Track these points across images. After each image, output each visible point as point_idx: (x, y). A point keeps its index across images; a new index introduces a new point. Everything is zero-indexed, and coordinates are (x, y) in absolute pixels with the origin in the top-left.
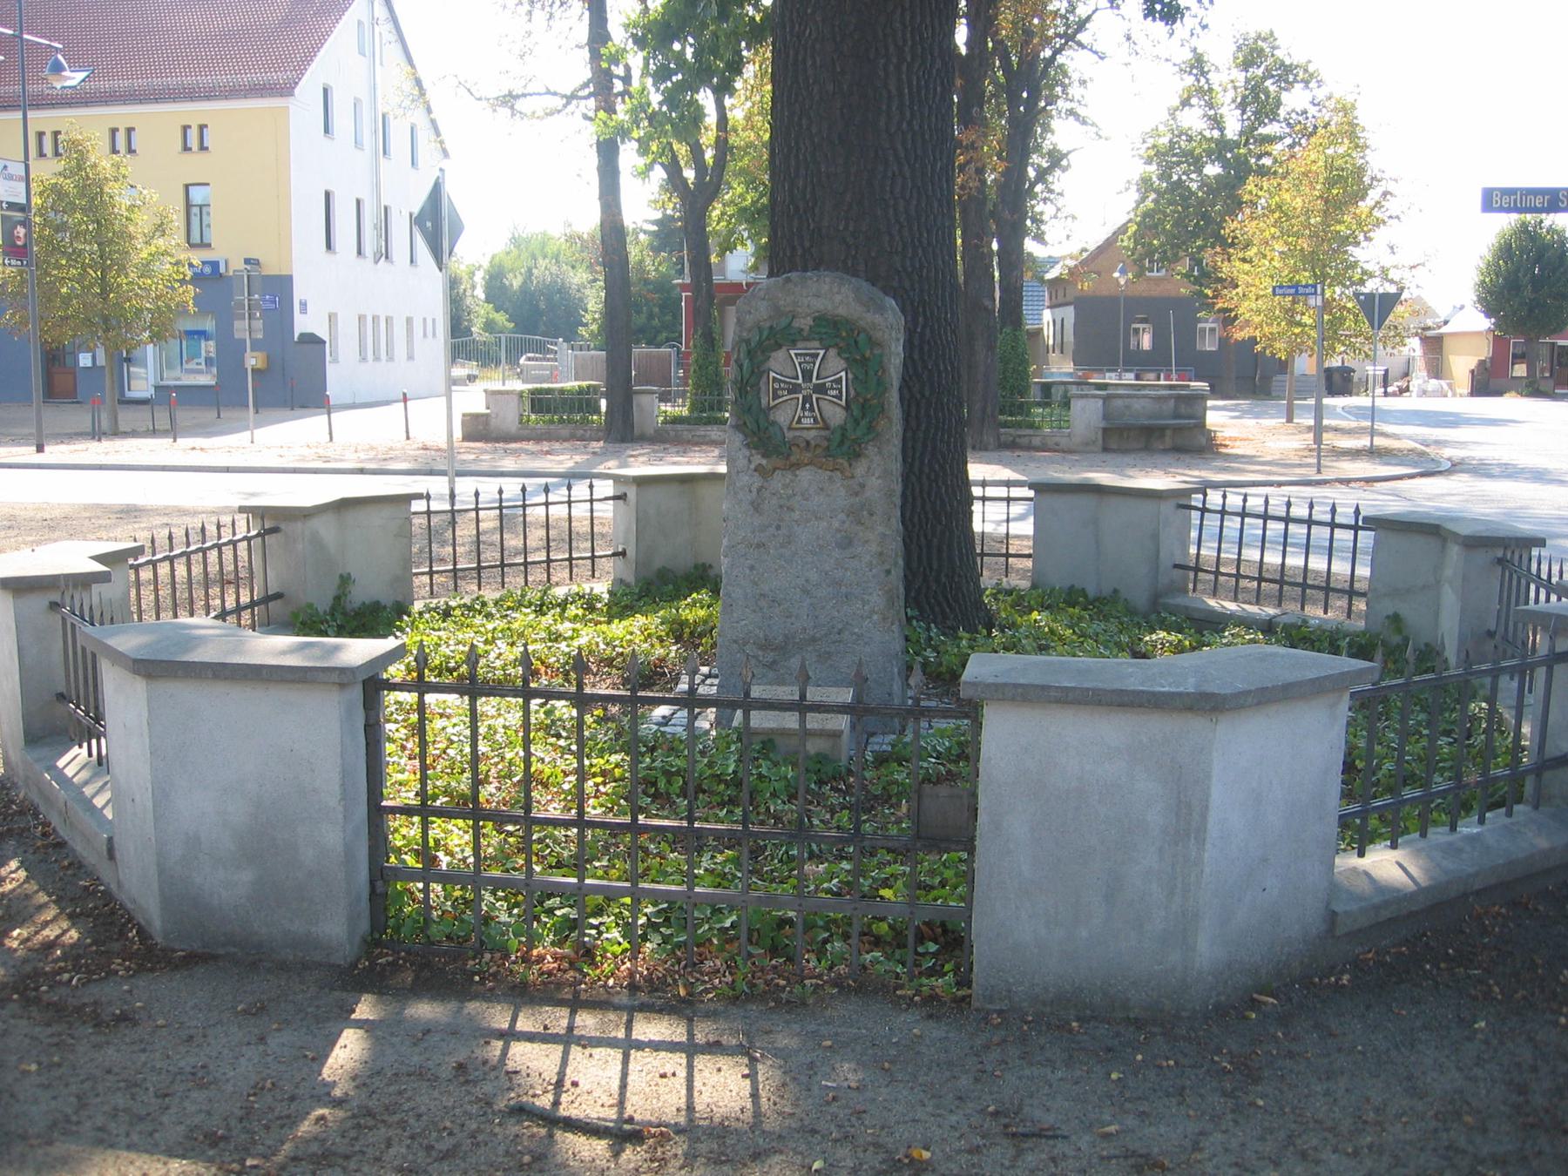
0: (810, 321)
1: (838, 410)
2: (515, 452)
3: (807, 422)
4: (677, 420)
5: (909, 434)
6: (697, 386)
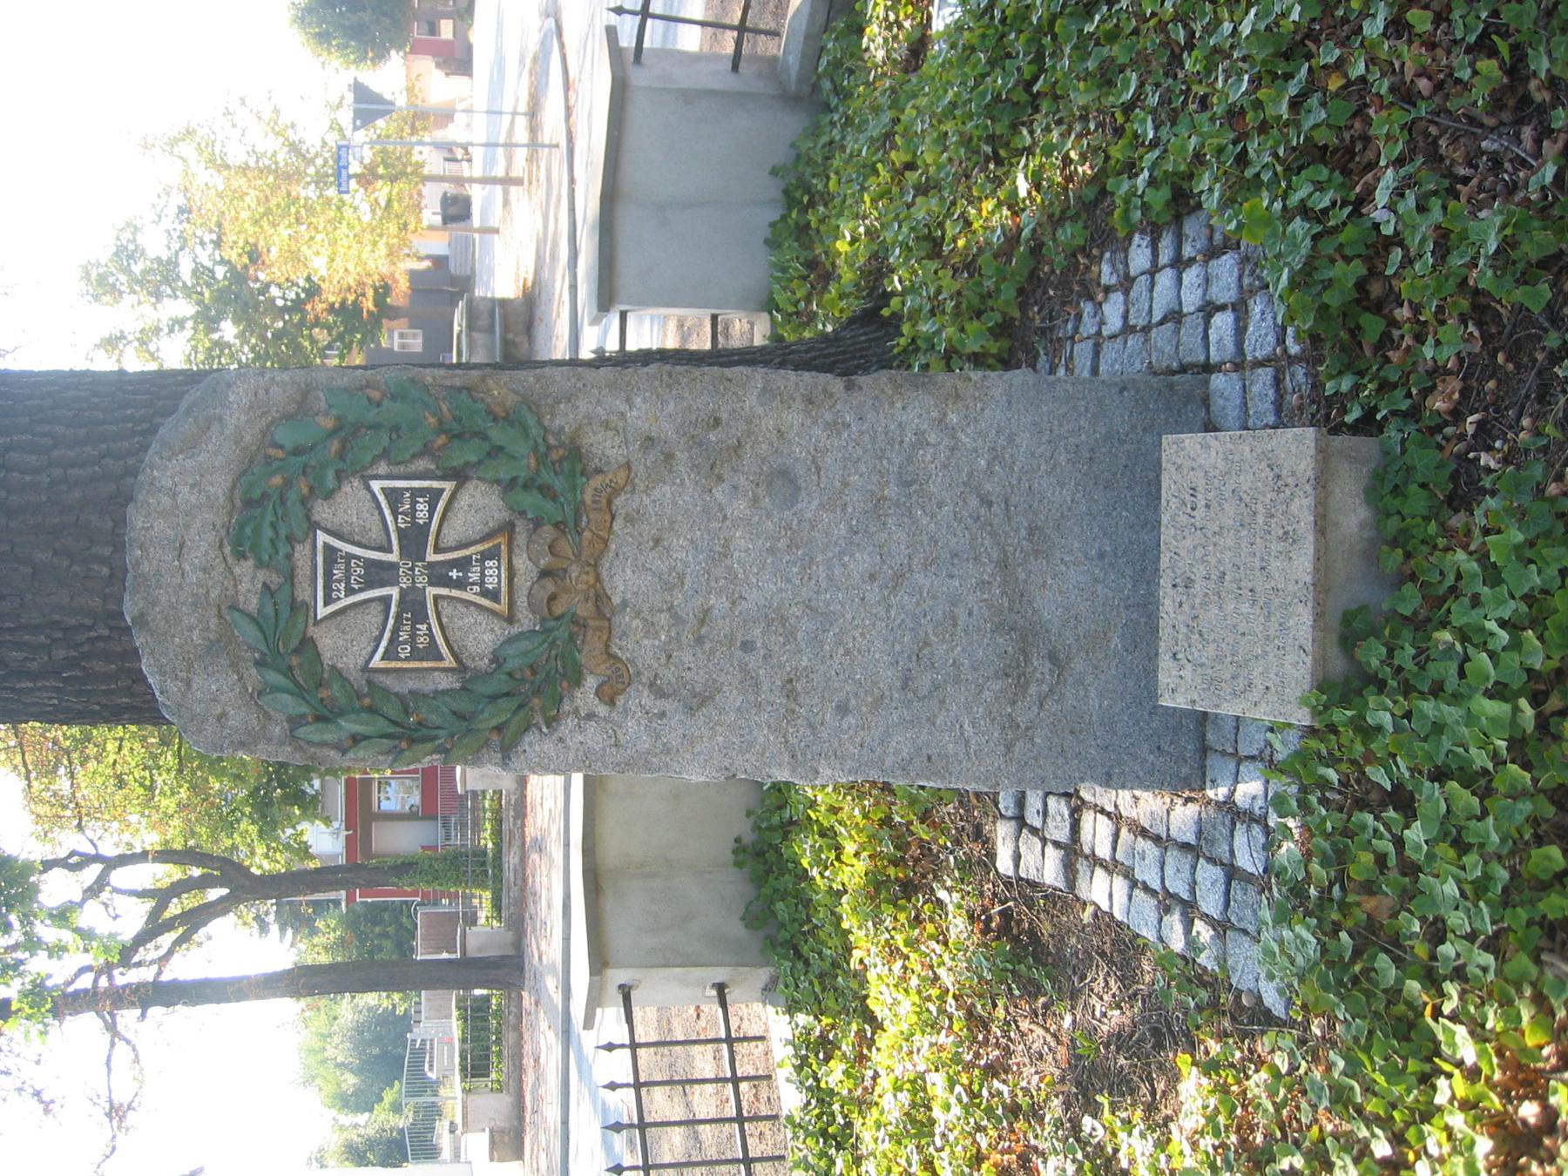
0: (245, 569)
1: (464, 500)
2: (537, 1099)
3: (494, 574)
4: (497, 905)
6: (457, 882)
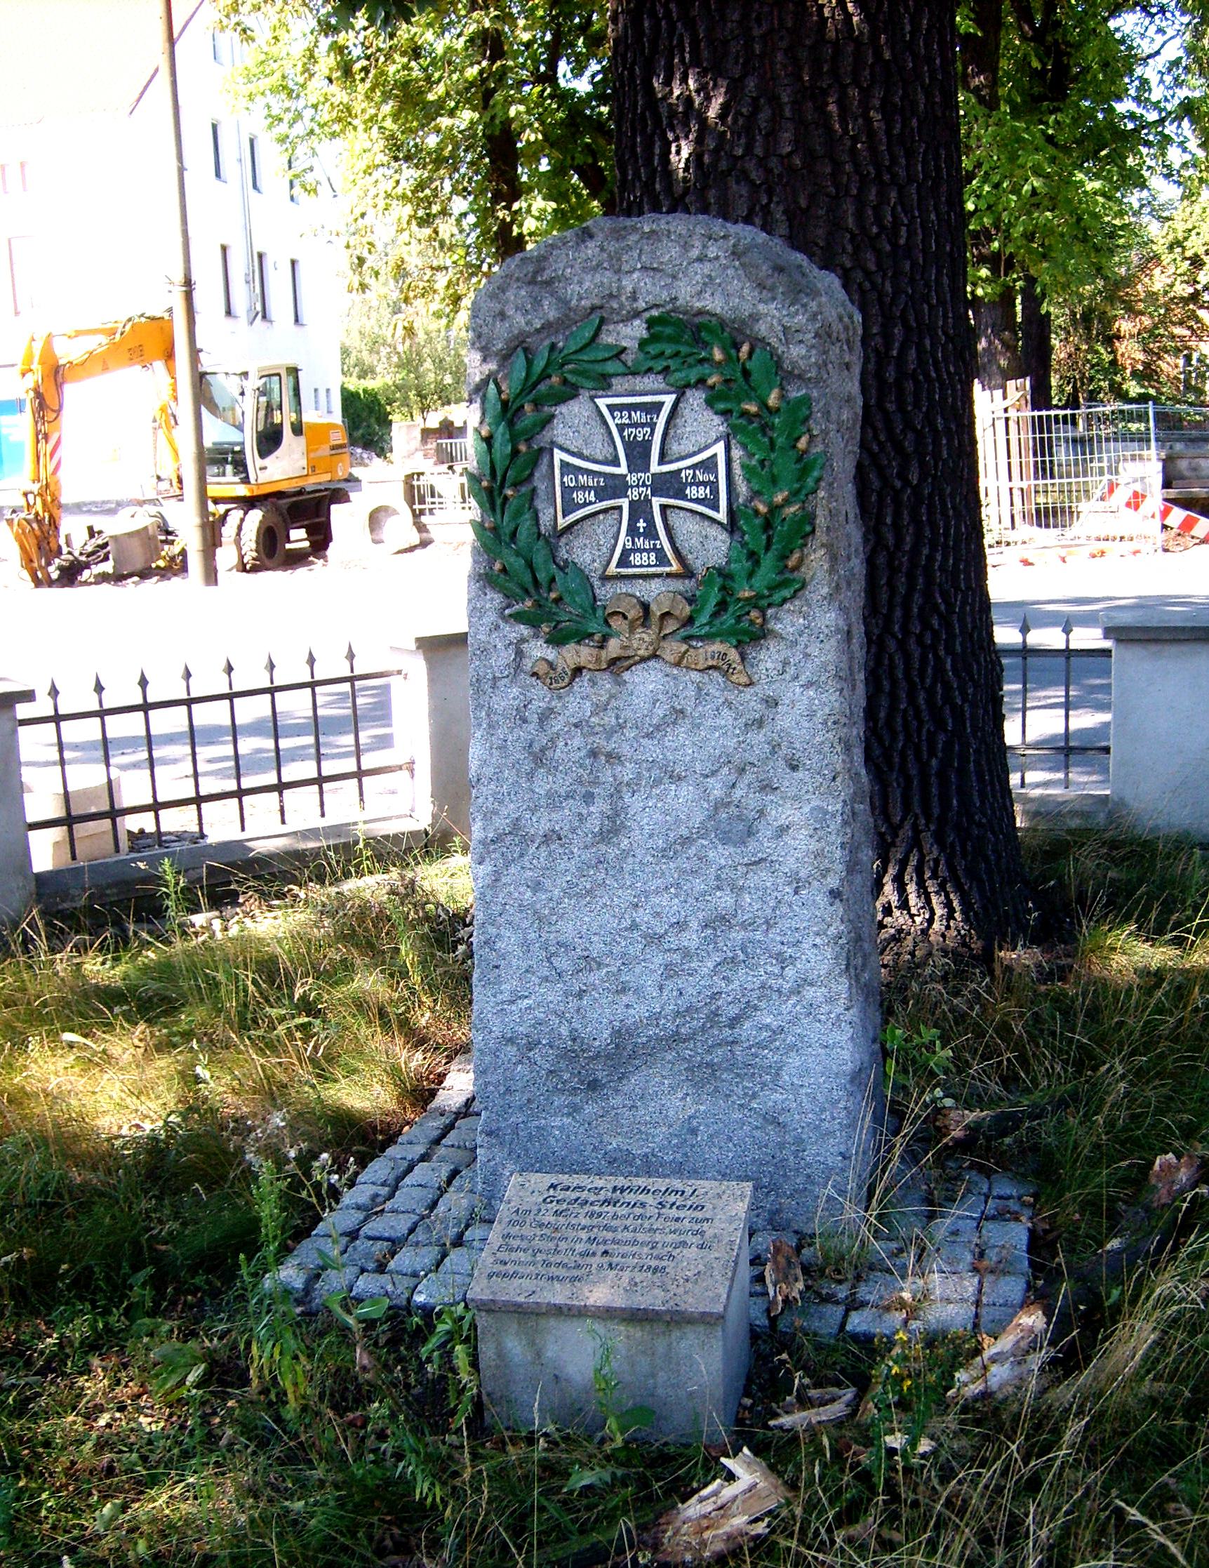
0: (637, 329)
1: (713, 531)
5: (881, 560)
